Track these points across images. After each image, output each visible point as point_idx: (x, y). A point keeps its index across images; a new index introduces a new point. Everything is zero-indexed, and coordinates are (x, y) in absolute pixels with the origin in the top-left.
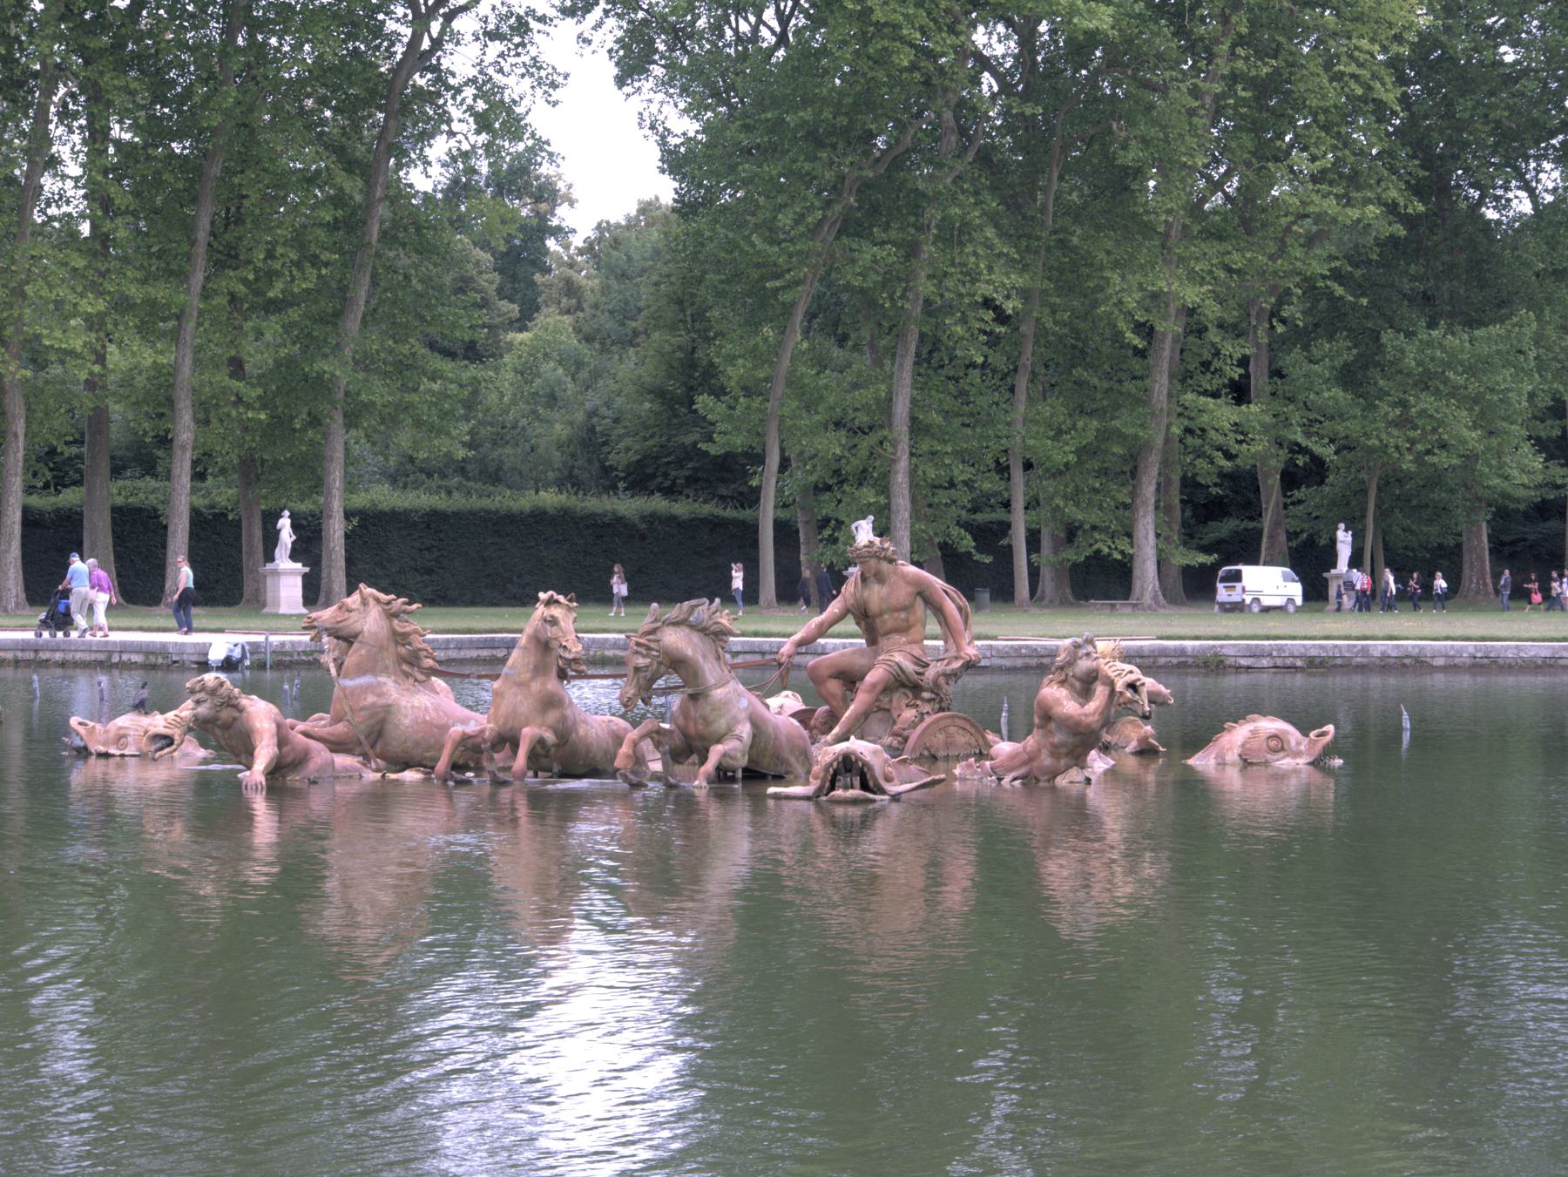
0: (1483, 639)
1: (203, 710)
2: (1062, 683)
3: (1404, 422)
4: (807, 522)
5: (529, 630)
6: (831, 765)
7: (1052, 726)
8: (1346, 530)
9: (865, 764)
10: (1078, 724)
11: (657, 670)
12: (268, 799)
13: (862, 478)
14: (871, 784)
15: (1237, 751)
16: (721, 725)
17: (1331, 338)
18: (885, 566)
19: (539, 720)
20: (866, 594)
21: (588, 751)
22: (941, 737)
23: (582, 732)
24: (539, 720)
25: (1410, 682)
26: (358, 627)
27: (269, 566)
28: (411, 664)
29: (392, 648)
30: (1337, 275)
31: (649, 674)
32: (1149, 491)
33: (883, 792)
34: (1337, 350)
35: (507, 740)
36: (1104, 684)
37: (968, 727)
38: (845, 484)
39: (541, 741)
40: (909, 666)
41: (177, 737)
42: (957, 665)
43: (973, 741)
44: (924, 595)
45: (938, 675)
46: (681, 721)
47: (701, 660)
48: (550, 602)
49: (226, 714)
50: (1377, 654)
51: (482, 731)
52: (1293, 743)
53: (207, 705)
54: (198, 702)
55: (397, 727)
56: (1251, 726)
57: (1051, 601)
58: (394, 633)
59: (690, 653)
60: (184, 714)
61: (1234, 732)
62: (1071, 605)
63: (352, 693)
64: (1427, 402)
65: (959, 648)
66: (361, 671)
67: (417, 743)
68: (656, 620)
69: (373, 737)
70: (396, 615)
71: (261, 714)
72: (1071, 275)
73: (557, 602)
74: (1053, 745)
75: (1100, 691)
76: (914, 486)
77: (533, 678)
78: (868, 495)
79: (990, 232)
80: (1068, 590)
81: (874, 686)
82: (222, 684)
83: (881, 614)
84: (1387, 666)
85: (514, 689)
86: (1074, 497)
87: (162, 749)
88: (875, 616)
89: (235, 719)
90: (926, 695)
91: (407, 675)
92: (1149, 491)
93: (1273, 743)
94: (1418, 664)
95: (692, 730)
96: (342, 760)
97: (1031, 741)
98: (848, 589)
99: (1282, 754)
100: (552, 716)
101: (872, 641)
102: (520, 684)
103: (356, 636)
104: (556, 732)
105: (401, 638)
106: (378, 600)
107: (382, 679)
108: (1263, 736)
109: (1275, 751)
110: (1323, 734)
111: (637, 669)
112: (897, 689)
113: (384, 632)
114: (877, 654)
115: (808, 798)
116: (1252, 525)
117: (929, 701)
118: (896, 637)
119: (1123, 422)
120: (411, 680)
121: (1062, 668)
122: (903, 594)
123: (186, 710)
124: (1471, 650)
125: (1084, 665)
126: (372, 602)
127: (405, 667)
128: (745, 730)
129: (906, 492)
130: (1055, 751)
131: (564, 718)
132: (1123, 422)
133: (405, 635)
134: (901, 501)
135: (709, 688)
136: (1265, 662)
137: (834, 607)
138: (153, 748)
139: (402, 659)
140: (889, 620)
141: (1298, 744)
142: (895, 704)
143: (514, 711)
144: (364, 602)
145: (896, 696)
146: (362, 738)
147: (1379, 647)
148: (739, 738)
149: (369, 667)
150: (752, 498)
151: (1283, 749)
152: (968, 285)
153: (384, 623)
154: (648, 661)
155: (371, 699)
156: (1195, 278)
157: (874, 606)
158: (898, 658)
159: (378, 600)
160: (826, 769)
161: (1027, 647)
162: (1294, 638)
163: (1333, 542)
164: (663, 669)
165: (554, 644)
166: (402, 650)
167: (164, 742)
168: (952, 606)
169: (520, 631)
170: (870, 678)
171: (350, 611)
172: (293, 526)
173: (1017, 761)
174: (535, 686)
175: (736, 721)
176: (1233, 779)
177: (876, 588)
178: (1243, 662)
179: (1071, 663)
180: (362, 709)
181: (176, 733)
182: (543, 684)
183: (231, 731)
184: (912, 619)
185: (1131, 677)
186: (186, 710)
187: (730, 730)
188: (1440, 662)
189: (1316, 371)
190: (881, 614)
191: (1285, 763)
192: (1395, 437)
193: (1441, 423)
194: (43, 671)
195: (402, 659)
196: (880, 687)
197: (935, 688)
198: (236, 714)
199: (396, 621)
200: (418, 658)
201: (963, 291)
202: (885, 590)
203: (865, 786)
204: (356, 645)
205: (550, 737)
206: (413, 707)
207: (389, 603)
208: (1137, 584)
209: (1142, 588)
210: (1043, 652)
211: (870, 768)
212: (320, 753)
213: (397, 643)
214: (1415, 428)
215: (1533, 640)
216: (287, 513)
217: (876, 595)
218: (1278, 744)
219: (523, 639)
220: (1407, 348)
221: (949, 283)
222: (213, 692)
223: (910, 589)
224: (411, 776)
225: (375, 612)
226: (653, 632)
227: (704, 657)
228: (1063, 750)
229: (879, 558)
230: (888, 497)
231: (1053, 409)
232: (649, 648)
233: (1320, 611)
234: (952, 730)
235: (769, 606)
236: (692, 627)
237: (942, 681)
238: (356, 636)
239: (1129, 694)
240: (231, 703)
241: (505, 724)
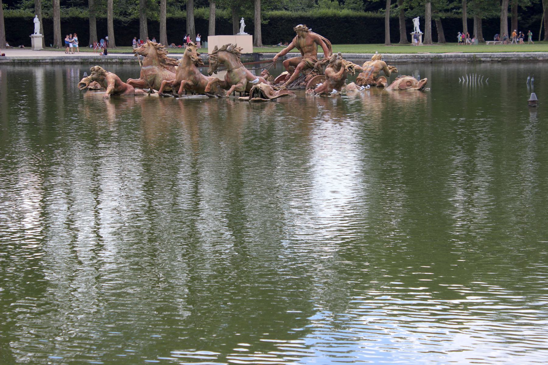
2: (332, 67)
5: (185, 53)
9: (261, 90)
10: (335, 78)
12: (111, 102)
15: (398, 86)
16: (237, 79)
18: (305, 33)
23: (202, 82)
25: (531, 66)
26: (147, 52)
28: (162, 63)
29: (157, 58)
31: (215, 65)
33: (268, 98)
35: (178, 84)
39: (187, 84)
40: (311, 62)
44: (317, 42)
45: (318, 65)
47: (230, 61)
51: (173, 82)
52: (414, 84)
56: (402, 79)
59: (227, 59)
65: (326, 57)
66: (148, 64)
70: (158, 49)
71: (111, 77)
75: (342, 69)
81: (300, 68)
83: (304, 47)
84: (519, 61)
91: (162, 66)
93: (408, 84)
94: (534, 60)
95: (229, 81)
96: (137, 90)
97: (325, 83)
98: (295, 39)
100: (192, 78)
101: (303, 54)
104: (193, 81)
105: (159, 55)
109: (408, 86)
110: (424, 81)
111: (212, 64)
112: (307, 69)
113: (155, 53)
117: (316, 72)
121: (332, 62)
122: (310, 41)
125: (337, 61)
126: (151, 45)
128: (244, 81)
131: (195, 78)
133: (161, 54)
136: (488, 59)
137: (291, 45)
140: (306, 49)
141: (416, 84)
144: (149, 45)
145: (307, 71)
147: (522, 54)
148: (242, 83)
149: (150, 63)
153: (154, 51)
155: (150, 72)
157: (302, 45)
158: (308, 60)
159: (152, 44)
162: (539, 52)
168: (325, 44)
170: (299, 65)
172: (245, 22)
173: (321, 89)
175: (241, 78)
176: (397, 96)
177: (302, 39)
178: (482, 59)
179: (334, 61)
182: (189, 68)
185: (350, 65)
188: (541, 59)
190: (304, 47)
191: (412, 89)
196: (302, 68)
202: (305, 40)
203: (262, 96)
205: (190, 83)
207: (156, 45)
211: (263, 91)
212: (131, 88)
216: (243, 18)
217: (303, 41)
218: (410, 83)
223: (312, 40)
225: (152, 48)
226: (216, 53)
227: (232, 60)
233: (30, 49)
236: (228, 52)
240: (102, 74)
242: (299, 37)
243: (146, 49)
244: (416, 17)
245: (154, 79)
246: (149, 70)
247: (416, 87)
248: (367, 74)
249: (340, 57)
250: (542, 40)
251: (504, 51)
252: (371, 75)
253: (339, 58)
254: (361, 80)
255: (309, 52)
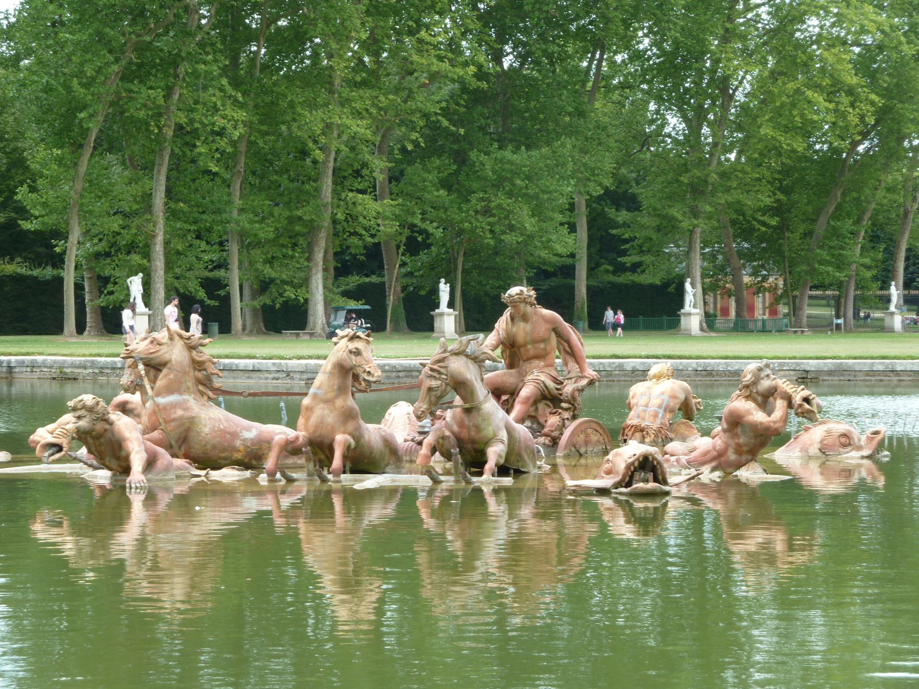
0: (680, 357)
1: (83, 423)
2: (747, 397)
3: (487, 212)
4: (90, 278)
6: (633, 463)
7: (739, 430)
8: (445, 284)
11: (445, 390)
13: (131, 248)
14: (660, 478)
17: (439, 157)
19: (342, 429)
20: (514, 330)
21: (371, 453)
22: (582, 436)
24: (342, 429)
26: (167, 357)
27: (437, 311)
30: (445, 112)
31: (439, 393)
32: (319, 256)
34: (441, 165)
36: (782, 398)
37: (598, 429)
38: (118, 252)
40: (551, 385)
41: (64, 445)
42: (584, 382)
43: (601, 439)
45: (574, 390)
46: (455, 428)
48: (353, 338)
49: (100, 426)
50: (629, 368)
51: (297, 438)
52: (856, 440)
53: (87, 419)
54: (79, 418)
55: (198, 433)
57: (251, 331)
58: (193, 361)
59: (469, 376)
60: (68, 427)
61: (811, 431)
62: (265, 333)
63: (165, 408)
64: (501, 199)
66: (169, 390)
67: (214, 447)
68: (445, 351)
69: (181, 441)
72: (269, 114)
73: (358, 337)
74: (739, 445)
76: (167, 255)
77: (336, 397)
78: (136, 258)
79: (224, 81)
80: (262, 324)
81: (528, 398)
82: (97, 404)
83: (525, 345)
85: (321, 405)
86: (270, 261)
87: (52, 454)
88: (519, 347)
89: (106, 430)
90: (564, 405)
91: (202, 394)
92: (319, 256)
93: (843, 440)
95: (464, 434)
99: (850, 448)
100: (350, 426)
102: (326, 401)
103: (165, 364)
105: (198, 365)
106: (181, 336)
107: (186, 397)
108: (836, 434)
109: (844, 446)
111: (430, 389)
114: (522, 375)
115: (603, 492)
116: (374, 279)
117: (566, 410)
118: (536, 362)
119: (305, 212)
120: (205, 398)
121: (747, 387)
122: (543, 330)
123: (68, 421)
124: (694, 366)
125: (765, 384)
126: (177, 338)
127: (201, 388)
128: (504, 435)
129: (162, 257)
130: (739, 450)
132: (305, 212)
134: (158, 264)
135: (481, 403)
138: (46, 454)
139: (199, 382)
142: (540, 412)
143: (322, 422)
146: (173, 442)
150: (58, 261)
151: (850, 444)
152: (209, 118)
154: (439, 382)
155: (180, 413)
156: (358, 114)
157: (520, 339)
160: (628, 467)
161: (389, 365)
163: (435, 291)
164: (449, 388)
165: (359, 371)
166: (200, 375)
167: (55, 449)
169: (325, 358)
171: (160, 344)
173: (708, 457)
174: (339, 402)
177: (522, 325)
180: (174, 420)
181: (64, 442)
183: (102, 440)
184: (548, 348)
186: (68, 421)
187: (495, 435)
189: (427, 176)
190: (525, 345)
192: (483, 222)
193: (510, 212)
194: (227, 397)
195: (199, 382)
197: (572, 401)
198: (107, 427)
199: (194, 352)
200: (210, 380)
201: (206, 122)
202: (528, 327)
204: (165, 371)
206: (210, 418)
208: (311, 319)
209: (315, 323)
210: (400, 368)
213: (195, 369)
214: (493, 215)
215: (855, 358)
219: (327, 365)
220: (486, 161)
221: (197, 116)
222: (90, 410)
223: (548, 326)
224: (228, 475)
228: (745, 449)
229: (526, 303)
230: (149, 261)
231: (262, 202)
232: (440, 373)
233: (429, 338)
234: (590, 431)
235: (71, 336)
236: (467, 356)
237: (577, 394)
238: (165, 364)
239: (807, 406)
241: (315, 432)
242: (512, 318)
243: (164, 349)
244: (136, 274)
245: (188, 430)
246: (174, 406)
247: (859, 448)
248: (656, 415)
249: (768, 371)
250: (81, 328)
251: (595, 354)
252: (663, 417)
253: (768, 376)
254: (642, 430)
255: (538, 357)
